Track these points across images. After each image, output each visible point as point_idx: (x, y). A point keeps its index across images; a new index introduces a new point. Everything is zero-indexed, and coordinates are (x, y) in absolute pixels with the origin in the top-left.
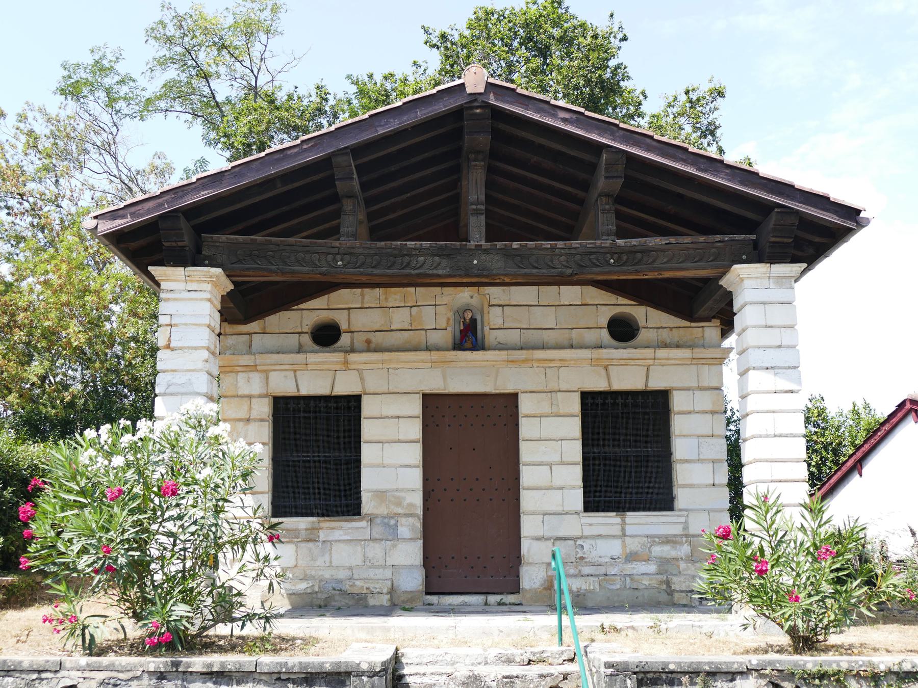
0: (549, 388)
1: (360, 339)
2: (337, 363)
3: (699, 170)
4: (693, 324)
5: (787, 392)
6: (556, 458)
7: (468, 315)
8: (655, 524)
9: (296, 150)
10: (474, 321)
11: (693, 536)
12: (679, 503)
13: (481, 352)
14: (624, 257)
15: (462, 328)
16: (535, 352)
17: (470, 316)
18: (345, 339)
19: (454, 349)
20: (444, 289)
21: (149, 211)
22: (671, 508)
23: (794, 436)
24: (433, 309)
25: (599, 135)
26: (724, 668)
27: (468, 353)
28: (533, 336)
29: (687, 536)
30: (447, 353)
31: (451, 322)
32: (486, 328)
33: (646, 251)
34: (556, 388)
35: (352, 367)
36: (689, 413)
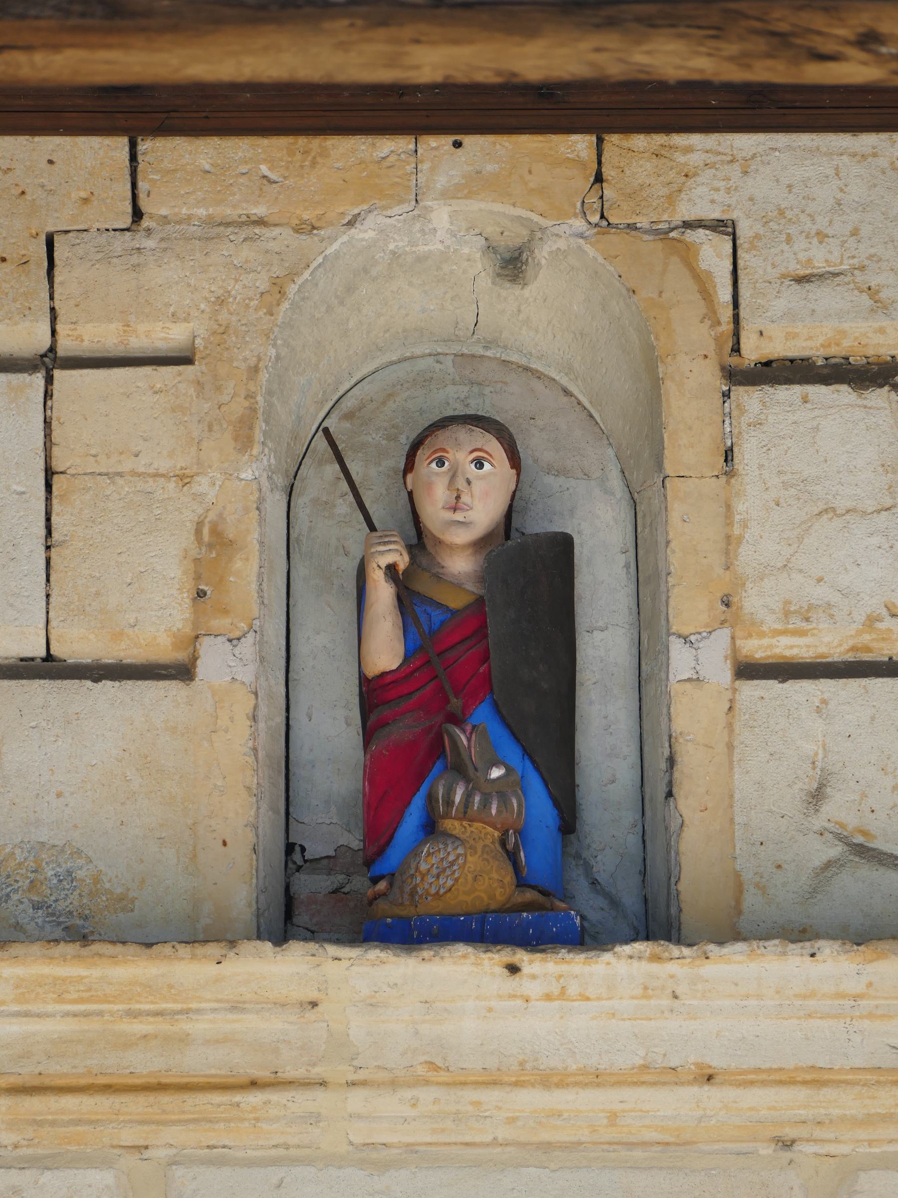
7: (468, 499)
10: (535, 571)
13: (624, 968)
15: (386, 652)
17: (484, 510)
19: (287, 919)
20: (164, 152)
27: (461, 975)
30: (188, 971)
31: (250, 576)
32: (697, 665)
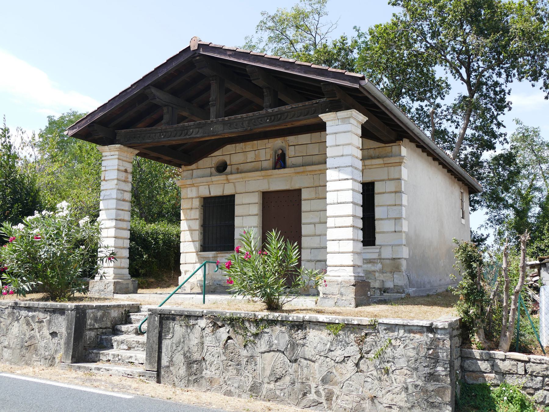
0: (315, 185)
1: (235, 167)
2: (224, 180)
3: (286, 69)
4: (386, 145)
5: (345, 179)
6: (317, 220)
7: (280, 152)
8: (368, 252)
9: (130, 90)
11: (384, 259)
12: (377, 242)
14: (273, 118)
16: (307, 167)
18: (229, 169)
19: (275, 168)
21: (84, 125)
22: (374, 245)
23: (348, 203)
24: (264, 150)
25: (244, 60)
26: (193, 314)
28: (308, 159)
29: (380, 259)
33: (282, 113)
34: (318, 185)
35: (231, 181)
36: (384, 193)
